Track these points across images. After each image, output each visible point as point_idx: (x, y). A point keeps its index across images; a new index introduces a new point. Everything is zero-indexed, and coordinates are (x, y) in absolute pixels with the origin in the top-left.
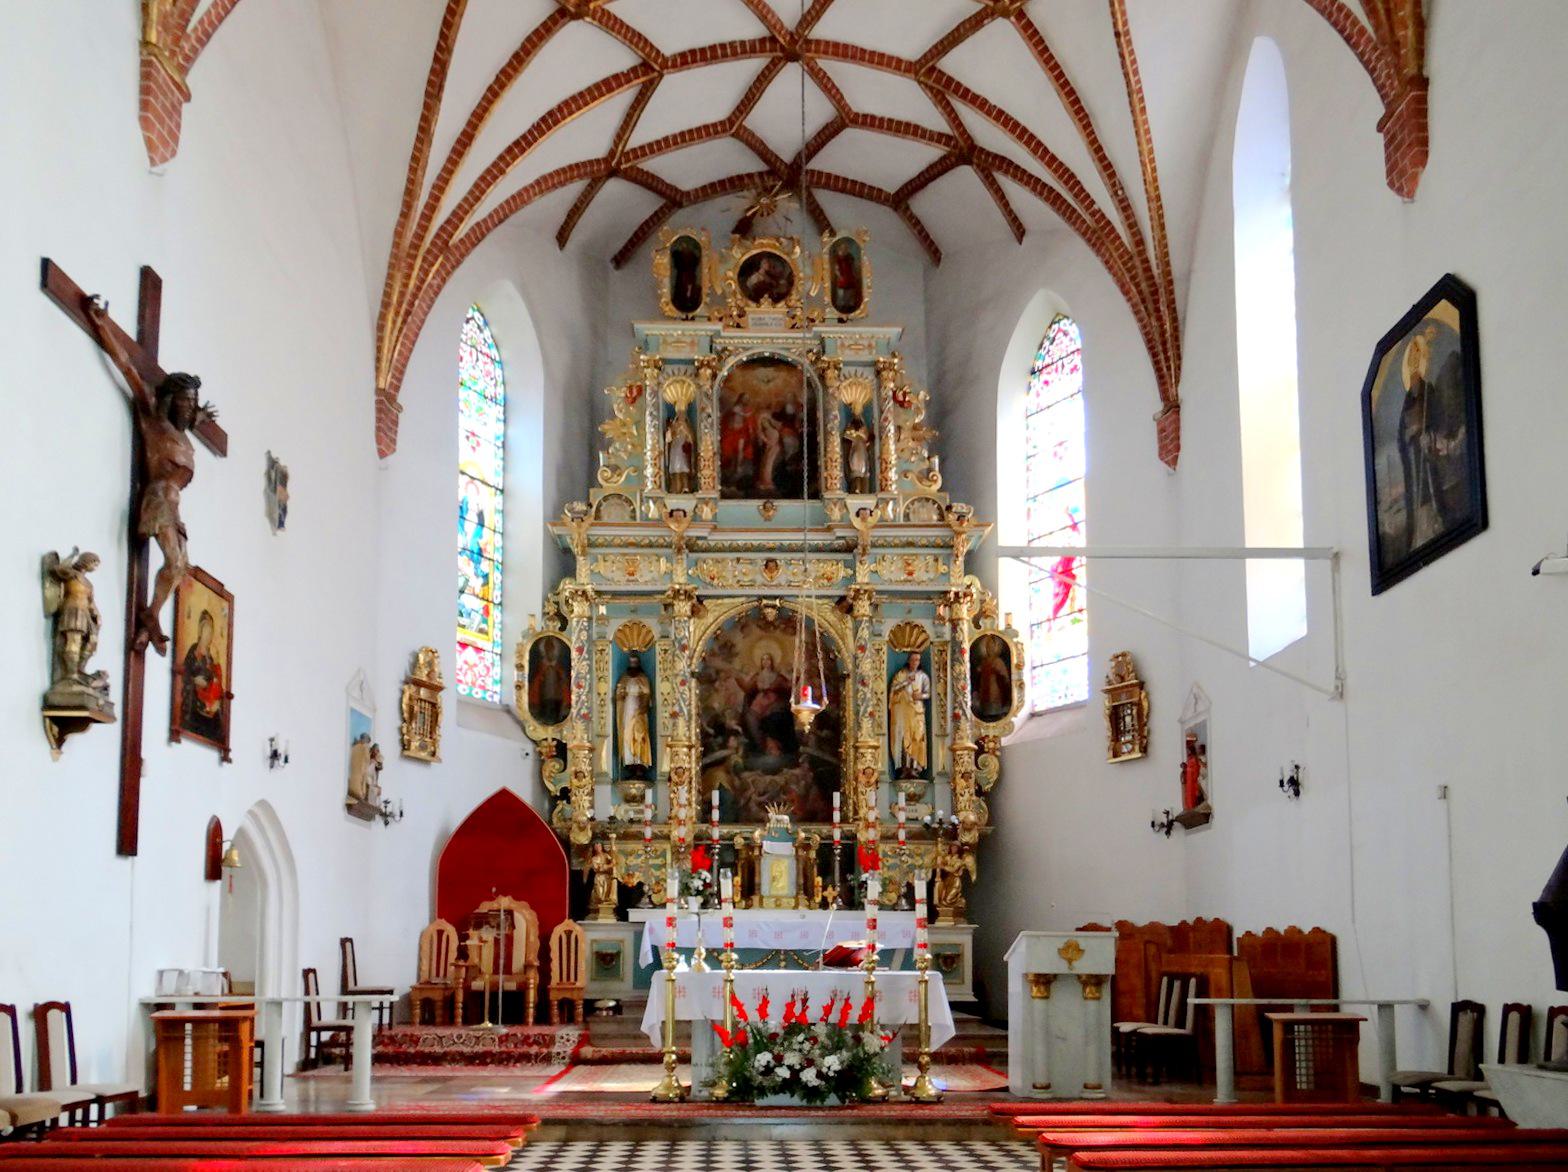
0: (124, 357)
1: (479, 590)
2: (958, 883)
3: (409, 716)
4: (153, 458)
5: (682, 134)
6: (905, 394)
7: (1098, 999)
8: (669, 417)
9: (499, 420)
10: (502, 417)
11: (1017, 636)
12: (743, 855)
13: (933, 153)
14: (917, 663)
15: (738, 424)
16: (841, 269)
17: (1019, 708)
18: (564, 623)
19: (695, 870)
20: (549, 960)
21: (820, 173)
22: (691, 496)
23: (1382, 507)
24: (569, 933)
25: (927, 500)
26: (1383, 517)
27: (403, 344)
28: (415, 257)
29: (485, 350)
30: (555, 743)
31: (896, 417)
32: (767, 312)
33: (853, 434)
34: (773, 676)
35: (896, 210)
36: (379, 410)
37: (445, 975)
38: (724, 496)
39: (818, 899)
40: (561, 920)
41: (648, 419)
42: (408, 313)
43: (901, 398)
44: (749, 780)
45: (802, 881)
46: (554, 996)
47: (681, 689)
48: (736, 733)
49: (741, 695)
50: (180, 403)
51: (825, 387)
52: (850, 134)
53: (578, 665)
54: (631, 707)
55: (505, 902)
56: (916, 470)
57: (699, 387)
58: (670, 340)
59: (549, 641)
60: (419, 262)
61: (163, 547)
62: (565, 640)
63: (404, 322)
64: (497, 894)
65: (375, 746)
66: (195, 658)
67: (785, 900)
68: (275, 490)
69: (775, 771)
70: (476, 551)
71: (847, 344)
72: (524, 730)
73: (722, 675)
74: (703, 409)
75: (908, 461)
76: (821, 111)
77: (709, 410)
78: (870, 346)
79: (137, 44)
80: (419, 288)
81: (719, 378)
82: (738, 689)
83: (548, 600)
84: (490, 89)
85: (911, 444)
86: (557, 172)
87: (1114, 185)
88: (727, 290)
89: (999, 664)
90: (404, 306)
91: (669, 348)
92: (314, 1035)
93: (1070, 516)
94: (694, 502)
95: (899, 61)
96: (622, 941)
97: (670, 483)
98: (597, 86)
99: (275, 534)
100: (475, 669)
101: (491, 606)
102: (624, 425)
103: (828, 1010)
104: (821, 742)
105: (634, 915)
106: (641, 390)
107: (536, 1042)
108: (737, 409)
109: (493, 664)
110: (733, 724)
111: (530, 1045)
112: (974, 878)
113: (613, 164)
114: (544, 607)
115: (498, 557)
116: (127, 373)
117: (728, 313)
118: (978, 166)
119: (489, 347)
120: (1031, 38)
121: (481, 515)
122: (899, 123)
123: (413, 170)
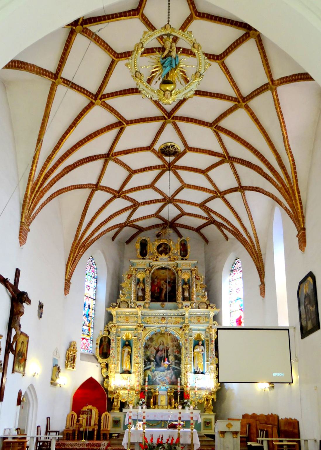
0: (11, 290)
1: (87, 325)
2: (211, 401)
3: (68, 358)
4: (15, 311)
5: (143, 217)
6: (198, 277)
7: (237, 437)
8: (138, 282)
9: (95, 282)
10: (96, 281)
12: (154, 394)
15: (156, 284)
18: (109, 333)
19: (141, 398)
20: (101, 422)
21: (178, 224)
22: (143, 302)
23: (302, 319)
24: (106, 415)
26: (302, 322)
27: (72, 268)
28: (76, 249)
29: (93, 266)
30: (105, 364)
31: (196, 282)
32: (164, 257)
33: (185, 286)
36: (65, 285)
37: (73, 427)
38: (152, 301)
39: (173, 407)
40: (104, 412)
41: (133, 283)
42: (74, 261)
43: (197, 277)
44: (156, 374)
45: (169, 401)
46: (102, 432)
48: (153, 361)
49: (155, 351)
50: (22, 298)
51: (178, 275)
52: (184, 217)
53: (113, 344)
54: (126, 354)
55: (90, 407)
56: (201, 295)
57: (146, 275)
59: (105, 337)
60: (77, 250)
61: (16, 330)
62: (109, 337)
63: (73, 263)
64: (88, 405)
65: (59, 367)
66: (19, 353)
67: (164, 407)
68: (40, 309)
70: (87, 314)
71: (184, 264)
72: (97, 360)
73: (150, 346)
74: (147, 281)
75: (199, 293)
76: (178, 185)
77: (148, 281)
79: (20, 222)
80: (77, 255)
81: (151, 272)
84: (97, 212)
85: (200, 289)
86: (112, 227)
87: (247, 233)
90: (73, 260)
91: (139, 266)
92: (38, 443)
93: (240, 307)
94: (144, 303)
95: (196, 203)
96: (121, 417)
97: (138, 298)
98: (123, 209)
99: (39, 320)
100: (86, 345)
101: (91, 328)
102: (127, 284)
103: (168, 440)
104: (176, 364)
105: (124, 410)
106: (131, 275)
107: (96, 446)
108: (156, 280)
110: (152, 359)
111: (94, 446)
112: (215, 401)
114: (104, 328)
115: (93, 316)
116: (12, 293)
117: (154, 257)
118: (216, 225)
120: (225, 202)
121: (89, 306)
122: (196, 215)
123: (77, 231)
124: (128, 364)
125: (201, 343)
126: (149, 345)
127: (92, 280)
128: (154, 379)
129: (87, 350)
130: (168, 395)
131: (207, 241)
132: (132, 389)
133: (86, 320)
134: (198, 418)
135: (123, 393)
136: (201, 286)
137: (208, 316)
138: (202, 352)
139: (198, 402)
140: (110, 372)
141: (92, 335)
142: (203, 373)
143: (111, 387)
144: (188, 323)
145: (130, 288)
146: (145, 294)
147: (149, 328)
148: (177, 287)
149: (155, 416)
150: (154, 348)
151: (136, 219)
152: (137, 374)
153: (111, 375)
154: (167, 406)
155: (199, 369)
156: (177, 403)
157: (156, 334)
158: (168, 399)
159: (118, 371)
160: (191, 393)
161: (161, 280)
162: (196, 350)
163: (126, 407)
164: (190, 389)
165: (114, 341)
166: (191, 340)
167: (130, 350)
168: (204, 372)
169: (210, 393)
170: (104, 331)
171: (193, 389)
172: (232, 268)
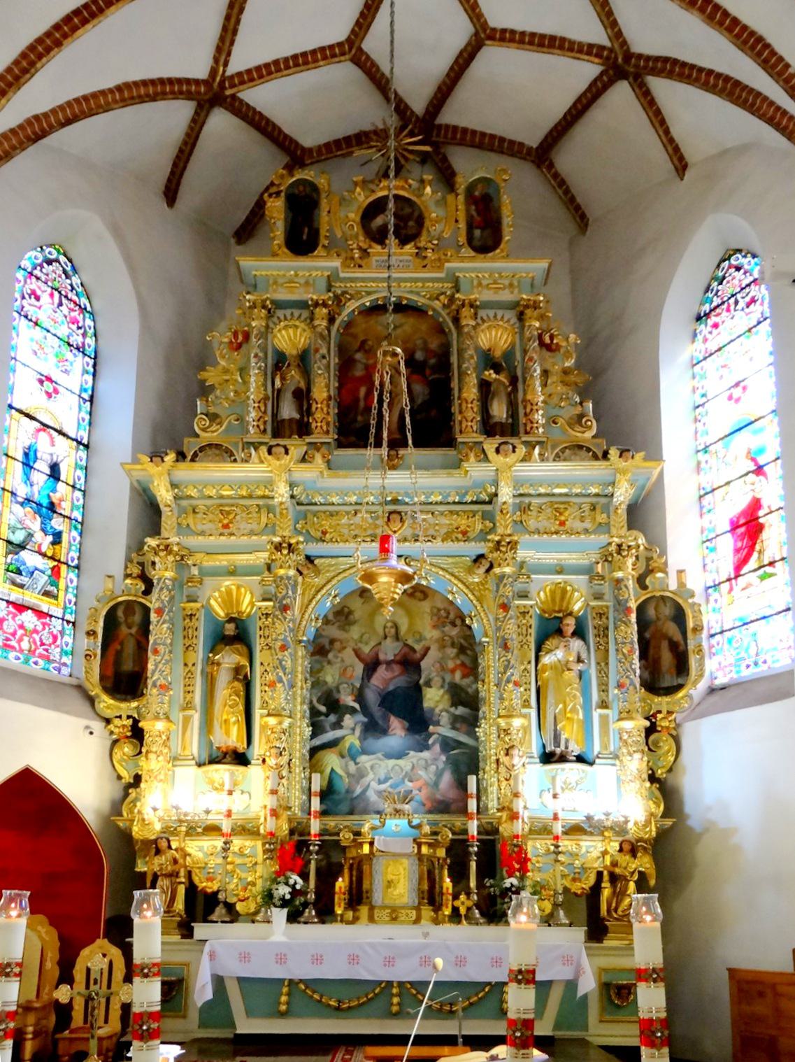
5: (295, 57)
6: (552, 337)
10: (91, 369)
11: (692, 596)
13: (589, 70)
14: (570, 629)
15: (359, 372)
16: (477, 210)
17: (695, 683)
21: (455, 128)
25: (580, 447)
30: (130, 722)
31: (542, 360)
34: (399, 645)
35: (539, 166)
38: (340, 445)
39: (447, 912)
41: (253, 361)
43: (547, 340)
44: (368, 765)
45: (426, 887)
49: (359, 668)
52: (493, 58)
53: (160, 632)
56: (567, 416)
58: (280, 281)
59: (129, 606)
69: (400, 755)
70: (45, 502)
71: (485, 282)
73: (337, 645)
81: (337, 322)
83: (131, 561)
89: (672, 629)
91: (280, 289)
93: (753, 460)
98: (67, 19)
101: (64, 568)
104: (455, 722)
106: (247, 336)
108: (358, 356)
109: (62, 632)
110: (348, 700)
113: (216, 85)
114: (126, 567)
119: (77, 295)
122: (543, 36)
125: (570, 625)
126: (332, 642)
127: (69, 356)
128: (358, 790)
130: (420, 856)
131: (580, 217)
132: (246, 829)
133: (35, 525)
134: (578, 972)
135: (199, 850)
137: (603, 500)
138: (580, 666)
139: (566, 890)
141: (71, 596)
142: (580, 759)
143: (143, 820)
144: (509, 531)
146: (309, 413)
147: (333, 561)
148: (455, 384)
149: (353, 959)
150: (357, 653)
151: (258, 69)
152: (271, 762)
154: (418, 909)
155: (567, 741)
156: (468, 894)
158: (421, 879)
160: (536, 848)
162: (547, 660)
163: (213, 917)
164: (527, 828)
165: (166, 617)
166: (524, 614)
167: (245, 662)
168: (590, 757)
169: (627, 847)
170: (127, 576)
171: (542, 829)
172: (702, 304)
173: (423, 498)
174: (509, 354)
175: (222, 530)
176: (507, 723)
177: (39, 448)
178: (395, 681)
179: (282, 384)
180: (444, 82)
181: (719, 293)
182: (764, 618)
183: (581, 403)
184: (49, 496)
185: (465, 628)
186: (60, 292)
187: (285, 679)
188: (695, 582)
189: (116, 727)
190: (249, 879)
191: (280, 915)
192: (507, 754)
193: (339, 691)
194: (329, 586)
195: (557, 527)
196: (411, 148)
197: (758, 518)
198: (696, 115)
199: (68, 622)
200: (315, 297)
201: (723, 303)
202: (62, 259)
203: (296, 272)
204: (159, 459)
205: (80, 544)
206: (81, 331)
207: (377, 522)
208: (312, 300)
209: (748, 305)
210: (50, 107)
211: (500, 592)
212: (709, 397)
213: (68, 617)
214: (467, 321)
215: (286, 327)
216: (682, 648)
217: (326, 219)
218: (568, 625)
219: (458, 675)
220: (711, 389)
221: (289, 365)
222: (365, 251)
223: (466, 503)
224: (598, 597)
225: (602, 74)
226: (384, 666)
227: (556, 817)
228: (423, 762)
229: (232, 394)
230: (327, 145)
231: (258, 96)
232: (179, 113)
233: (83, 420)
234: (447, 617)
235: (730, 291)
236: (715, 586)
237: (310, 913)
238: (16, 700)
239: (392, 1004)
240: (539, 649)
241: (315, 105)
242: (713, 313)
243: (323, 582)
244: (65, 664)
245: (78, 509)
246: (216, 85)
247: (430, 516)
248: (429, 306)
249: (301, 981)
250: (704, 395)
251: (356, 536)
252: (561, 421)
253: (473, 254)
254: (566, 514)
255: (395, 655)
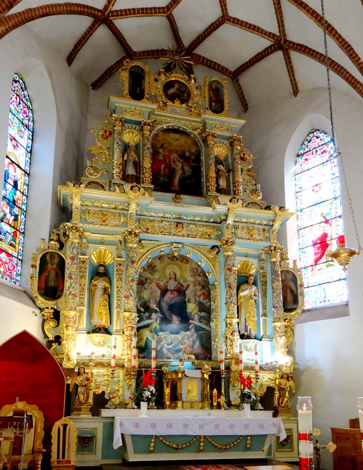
5: (142, 9)
6: (244, 155)
8: (126, 148)
13: (267, 43)
14: (252, 281)
15: (161, 157)
16: (213, 94)
21: (200, 56)
24: (65, 426)
25: (256, 203)
30: (53, 310)
34: (177, 283)
38: (155, 190)
44: (163, 337)
47: (131, 284)
49: (159, 292)
52: (226, 28)
53: (70, 268)
54: (99, 293)
57: (143, 135)
58: (128, 110)
59: (52, 255)
69: (177, 333)
70: (11, 199)
71: (217, 126)
73: (149, 281)
78: (228, 129)
81: (152, 133)
82: (157, 289)
88: (158, 94)
93: (324, 217)
96: (96, 429)
101: (18, 233)
104: (201, 319)
105: (105, 413)
108: (160, 150)
109: (17, 264)
110: (154, 306)
113: (106, 14)
114: (50, 236)
119: (26, 100)
121: (16, 183)
122: (250, 25)
124: (104, 313)
126: (146, 279)
127: (23, 129)
129: (8, 278)
136: (249, 173)
138: (256, 298)
140: (67, 326)
141: (20, 247)
145: (108, 157)
149: (186, 426)
150: (158, 285)
151: (125, 10)
153: (67, 332)
157: (160, 258)
159: (81, 327)
161: (171, 152)
162: (241, 294)
167: (108, 285)
172: (300, 150)
173: (192, 218)
174: (226, 159)
175: (102, 223)
176: (230, 321)
177: (10, 173)
178: (174, 299)
179: (127, 158)
180: (201, 35)
181: (308, 147)
182: (329, 282)
183: (256, 185)
184: (13, 197)
185: (205, 278)
186: (19, 97)
187: (133, 295)
188: (299, 265)
189: (45, 312)
190: (116, 388)
191: (247, 406)
192: (232, 334)
193: (149, 302)
194: (148, 254)
195: (249, 237)
196: (185, 61)
197: (326, 241)
198: (307, 69)
199: (20, 260)
200: (145, 121)
201: (310, 151)
202: (21, 81)
203: (135, 108)
204: (78, 185)
205: (25, 221)
206: (28, 118)
207: (171, 227)
208: (144, 121)
209: (322, 153)
210: (37, 6)
211: (228, 263)
212: (303, 189)
213: (19, 257)
214: (211, 142)
215: (128, 132)
216: (295, 293)
217: (148, 86)
218: (251, 280)
219: (202, 298)
220: (310, 187)
221: (130, 150)
222: (165, 103)
223: (210, 222)
224: (262, 268)
225: (271, 46)
226: (170, 292)
227: (257, 363)
228: (187, 336)
229: (104, 159)
230: (143, 52)
231: (121, 23)
232: (86, 22)
233: (28, 162)
234: (197, 272)
235: (314, 146)
236: (305, 268)
237: (152, 404)
238: (6, 297)
239: (200, 446)
240: (238, 289)
241: (143, 33)
242: (305, 154)
243: (145, 251)
244: (17, 280)
245: (24, 205)
246: (106, 14)
247: (195, 226)
248: (192, 133)
249: (161, 436)
250: (300, 188)
251: (162, 232)
252: (248, 191)
253: (212, 113)
254: (253, 232)
255: (175, 287)
